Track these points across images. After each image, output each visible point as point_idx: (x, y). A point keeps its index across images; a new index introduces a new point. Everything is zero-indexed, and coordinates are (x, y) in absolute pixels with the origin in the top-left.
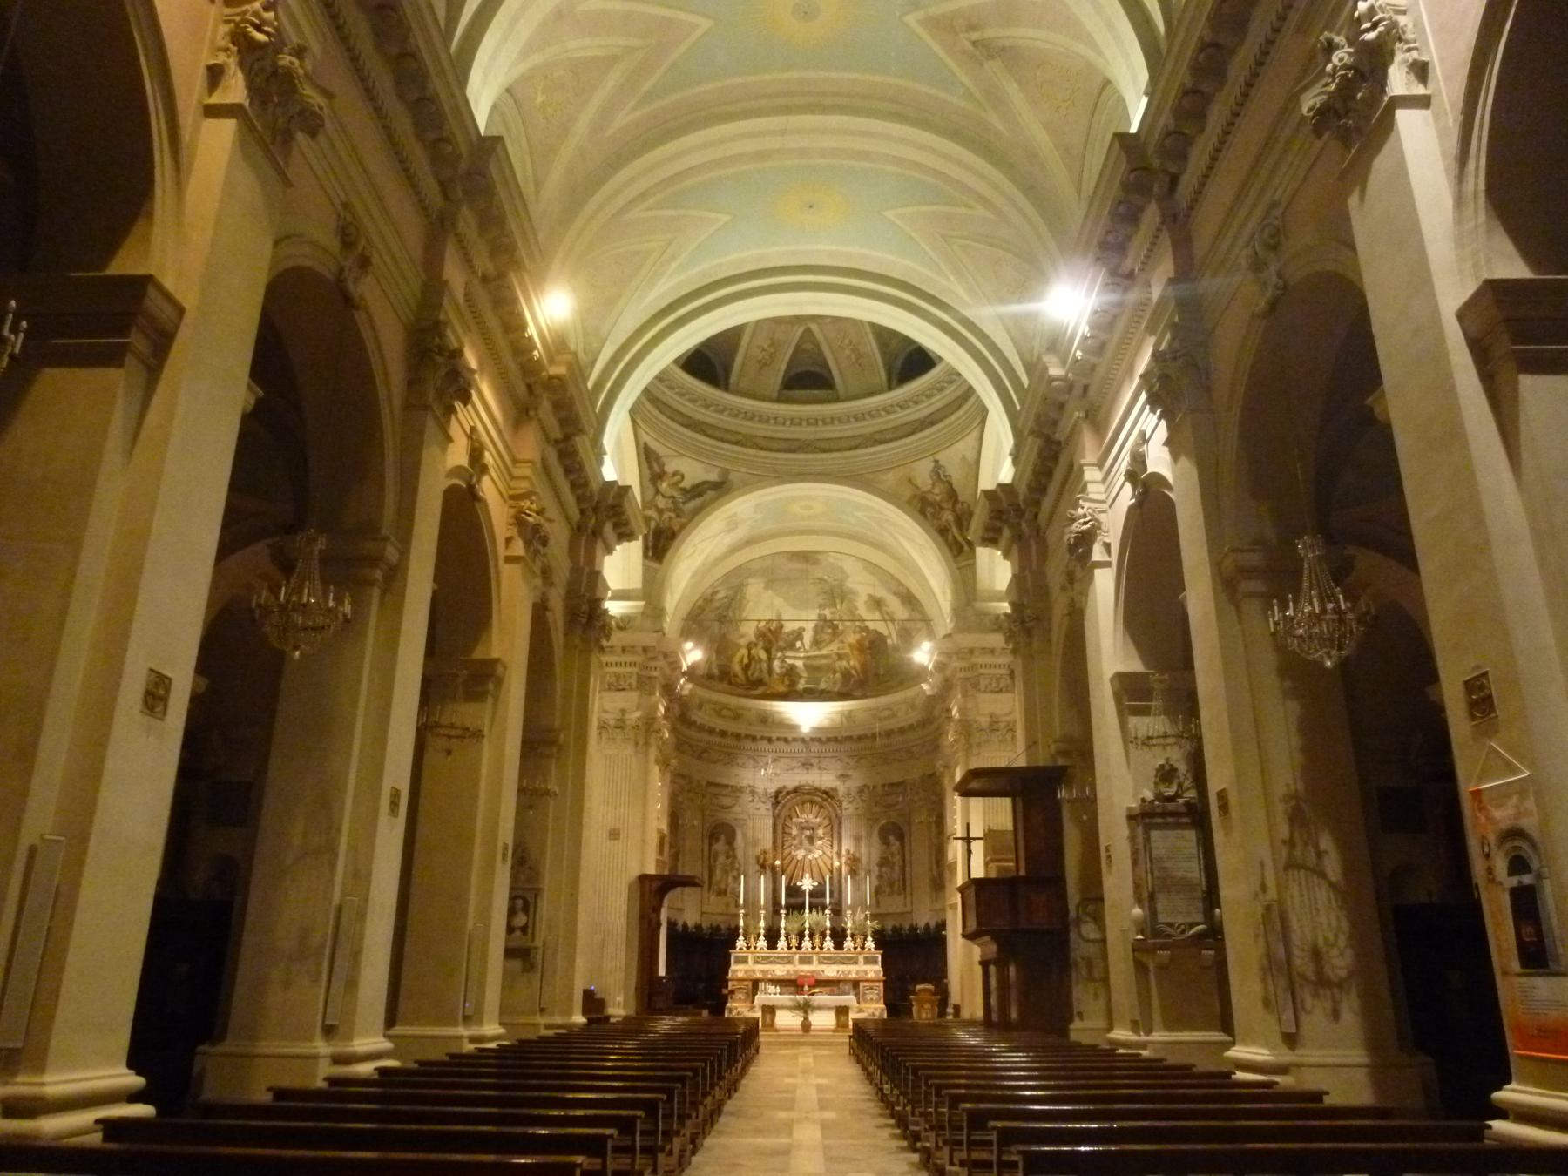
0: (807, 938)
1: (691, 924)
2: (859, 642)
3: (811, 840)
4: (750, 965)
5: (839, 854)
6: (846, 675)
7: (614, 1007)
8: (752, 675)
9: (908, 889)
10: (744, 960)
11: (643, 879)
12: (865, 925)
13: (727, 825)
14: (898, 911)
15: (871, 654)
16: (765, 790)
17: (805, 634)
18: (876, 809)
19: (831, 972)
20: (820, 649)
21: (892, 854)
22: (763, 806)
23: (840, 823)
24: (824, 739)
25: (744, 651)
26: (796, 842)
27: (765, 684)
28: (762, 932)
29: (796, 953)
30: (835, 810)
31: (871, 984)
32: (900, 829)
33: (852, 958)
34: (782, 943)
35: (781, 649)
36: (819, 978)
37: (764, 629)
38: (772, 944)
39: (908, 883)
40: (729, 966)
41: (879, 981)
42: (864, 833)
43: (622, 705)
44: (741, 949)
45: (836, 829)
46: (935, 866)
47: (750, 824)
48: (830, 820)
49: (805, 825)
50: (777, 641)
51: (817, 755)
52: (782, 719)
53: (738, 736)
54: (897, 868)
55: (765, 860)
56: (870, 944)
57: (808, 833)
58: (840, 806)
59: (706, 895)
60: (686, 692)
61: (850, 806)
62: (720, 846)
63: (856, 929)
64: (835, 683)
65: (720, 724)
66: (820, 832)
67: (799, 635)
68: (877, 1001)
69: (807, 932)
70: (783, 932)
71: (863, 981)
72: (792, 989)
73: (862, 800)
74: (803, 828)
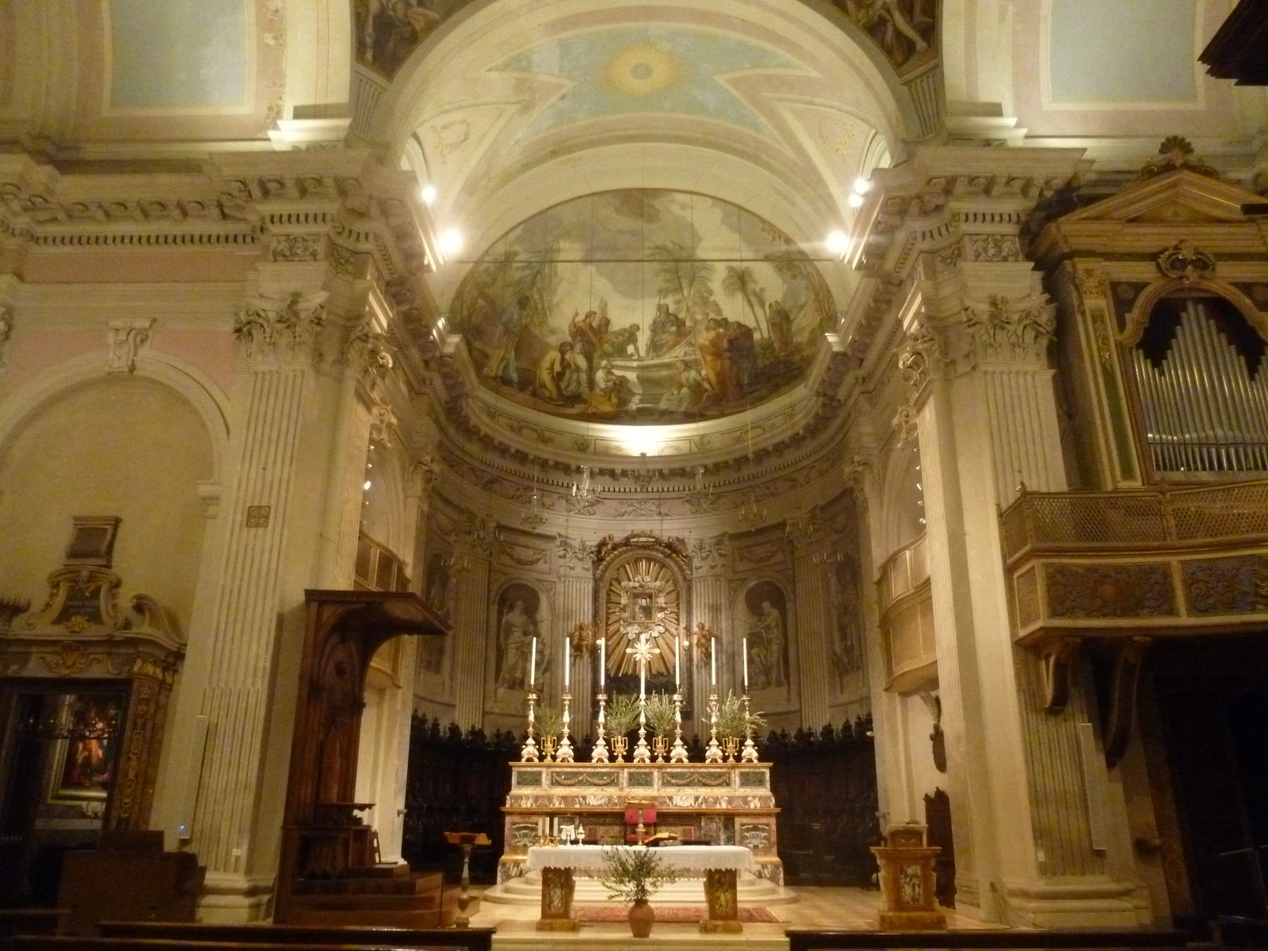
0: (642, 742)
1: (464, 728)
2: (714, 343)
3: (648, 611)
4: (545, 789)
5: (688, 629)
6: (697, 388)
7: (216, 869)
8: (568, 386)
9: (793, 678)
10: (535, 780)
11: (316, 598)
12: (742, 719)
13: (526, 587)
14: (779, 709)
15: (730, 358)
16: (583, 542)
17: (639, 334)
18: (741, 567)
19: (683, 799)
20: (659, 356)
21: (768, 628)
22: (579, 565)
23: (689, 589)
24: (666, 471)
25: (554, 355)
26: (626, 615)
27: (584, 401)
28: (566, 730)
29: (623, 768)
30: (682, 570)
31: (756, 821)
32: (778, 588)
33: (720, 775)
34: (600, 751)
35: (607, 355)
36: (664, 809)
37: (582, 324)
38: (582, 754)
39: (792, 671)
40: (509, 789)
41: (768, 815)
42: (724, 601)
43: (294, 286)
44: (529, 760)
45: (683, 606)
46: (836, 635)
47: (560, 587)
48: (675, 583)
49: (640, 590)
50: (601, 341)
51: (656, 495)
52: (607, 448)
53: (544, 464)
54: (775, 648)
55: (581, 638)
56: (750, 751)
57: (644, 602)
58: (689, 565)
59: (491, 686)
60: (449, 350)
61: (702, 564)
62: (515, 617)
63: (726, 725)
64: (680, 401)
65: (516, 442)
66: (661, 600)
67: (631, 335)
68: (766, 851)
69: (642, 732)
70: (601, 731)
71: (739, 815)
72: (616, 830)
73: (720, 555)
74: (636, 596)
